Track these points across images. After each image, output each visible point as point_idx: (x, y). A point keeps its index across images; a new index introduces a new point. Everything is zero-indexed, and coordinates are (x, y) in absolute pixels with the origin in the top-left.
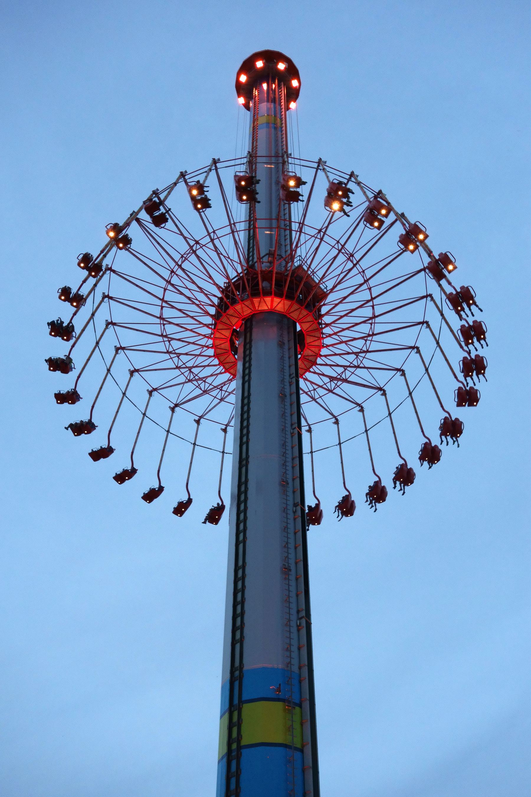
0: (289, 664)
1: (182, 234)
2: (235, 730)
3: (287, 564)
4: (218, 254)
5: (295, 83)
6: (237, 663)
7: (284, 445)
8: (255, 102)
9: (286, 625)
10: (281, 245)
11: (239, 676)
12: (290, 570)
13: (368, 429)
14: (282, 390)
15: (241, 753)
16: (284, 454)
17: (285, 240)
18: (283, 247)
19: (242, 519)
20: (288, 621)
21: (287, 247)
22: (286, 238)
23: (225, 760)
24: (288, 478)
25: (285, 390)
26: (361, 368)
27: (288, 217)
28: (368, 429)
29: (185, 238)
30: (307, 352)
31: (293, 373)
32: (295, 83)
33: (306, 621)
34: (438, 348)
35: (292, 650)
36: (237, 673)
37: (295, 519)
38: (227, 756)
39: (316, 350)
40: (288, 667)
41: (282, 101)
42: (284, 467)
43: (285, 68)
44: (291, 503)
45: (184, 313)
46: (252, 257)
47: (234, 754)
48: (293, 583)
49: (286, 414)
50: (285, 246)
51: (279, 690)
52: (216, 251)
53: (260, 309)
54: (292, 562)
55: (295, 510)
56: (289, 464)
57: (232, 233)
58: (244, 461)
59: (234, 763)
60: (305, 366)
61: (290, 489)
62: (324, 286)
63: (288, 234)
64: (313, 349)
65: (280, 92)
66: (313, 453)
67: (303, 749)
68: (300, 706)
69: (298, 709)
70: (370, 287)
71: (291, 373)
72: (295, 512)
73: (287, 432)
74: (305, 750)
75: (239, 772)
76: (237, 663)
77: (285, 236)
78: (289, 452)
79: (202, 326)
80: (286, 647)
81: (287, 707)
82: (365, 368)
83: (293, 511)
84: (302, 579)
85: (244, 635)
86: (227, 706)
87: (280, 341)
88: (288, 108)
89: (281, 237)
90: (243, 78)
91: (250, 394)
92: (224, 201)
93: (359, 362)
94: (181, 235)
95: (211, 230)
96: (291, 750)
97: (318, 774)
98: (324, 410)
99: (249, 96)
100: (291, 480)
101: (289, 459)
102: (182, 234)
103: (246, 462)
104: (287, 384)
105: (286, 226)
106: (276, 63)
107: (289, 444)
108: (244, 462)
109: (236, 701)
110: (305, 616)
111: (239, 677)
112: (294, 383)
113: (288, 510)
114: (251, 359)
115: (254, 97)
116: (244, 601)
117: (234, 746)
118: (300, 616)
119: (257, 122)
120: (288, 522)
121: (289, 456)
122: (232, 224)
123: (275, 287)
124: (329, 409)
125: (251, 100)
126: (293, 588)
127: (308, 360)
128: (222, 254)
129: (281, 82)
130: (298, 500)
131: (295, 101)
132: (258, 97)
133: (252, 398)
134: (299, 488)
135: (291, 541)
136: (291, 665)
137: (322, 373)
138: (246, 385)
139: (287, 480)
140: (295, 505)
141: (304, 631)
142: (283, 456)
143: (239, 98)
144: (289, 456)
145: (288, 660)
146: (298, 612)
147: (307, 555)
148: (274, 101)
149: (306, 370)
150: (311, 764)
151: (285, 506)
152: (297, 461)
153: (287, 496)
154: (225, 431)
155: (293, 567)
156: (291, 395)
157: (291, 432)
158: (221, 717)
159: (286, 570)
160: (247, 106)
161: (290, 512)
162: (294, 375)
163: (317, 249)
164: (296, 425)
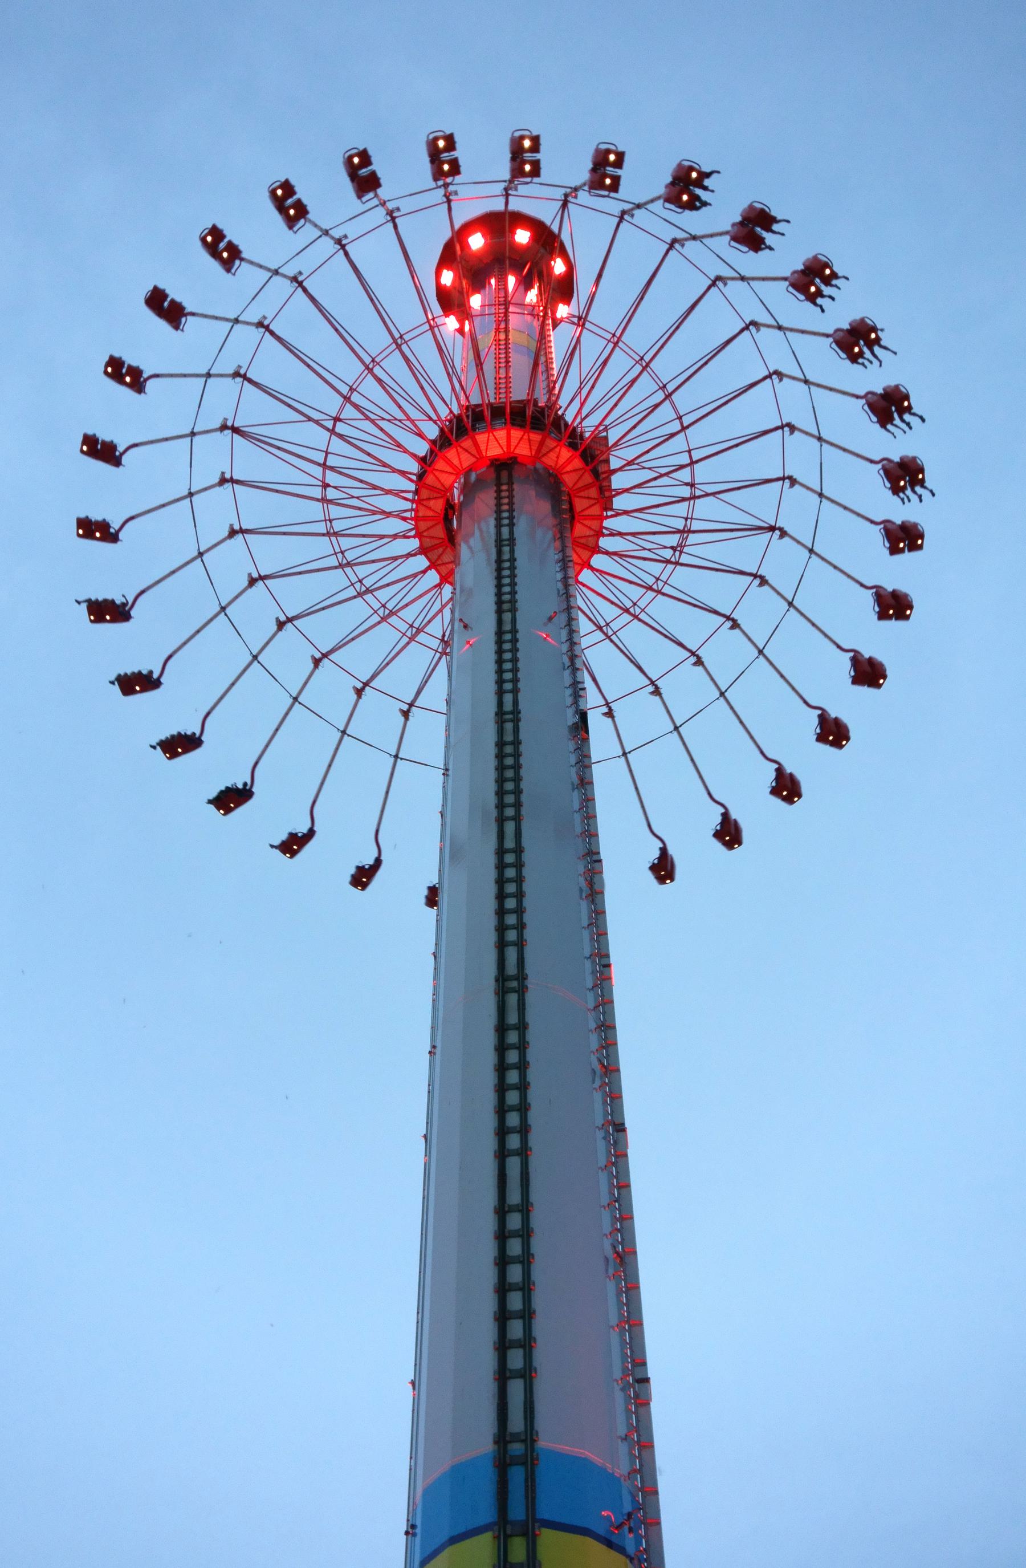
1: (310, 419)
13: (819, 491)
26: (699, 497)
28: (819, 491)
29: (317, 422)
30: (580, 530)
39: (594, 524)
45: (363, 414)
57: (397, 348)
70: (663, 383)
92: (372, 300)
95: (397, 335)
98: (735, 450)
102: (310, 419)
122: (398, 339)
123: (543, 268)
124: (746, 436)
127: (585, 547)
128: (389, 421)
137: (624, 537)
149: (583, 565)
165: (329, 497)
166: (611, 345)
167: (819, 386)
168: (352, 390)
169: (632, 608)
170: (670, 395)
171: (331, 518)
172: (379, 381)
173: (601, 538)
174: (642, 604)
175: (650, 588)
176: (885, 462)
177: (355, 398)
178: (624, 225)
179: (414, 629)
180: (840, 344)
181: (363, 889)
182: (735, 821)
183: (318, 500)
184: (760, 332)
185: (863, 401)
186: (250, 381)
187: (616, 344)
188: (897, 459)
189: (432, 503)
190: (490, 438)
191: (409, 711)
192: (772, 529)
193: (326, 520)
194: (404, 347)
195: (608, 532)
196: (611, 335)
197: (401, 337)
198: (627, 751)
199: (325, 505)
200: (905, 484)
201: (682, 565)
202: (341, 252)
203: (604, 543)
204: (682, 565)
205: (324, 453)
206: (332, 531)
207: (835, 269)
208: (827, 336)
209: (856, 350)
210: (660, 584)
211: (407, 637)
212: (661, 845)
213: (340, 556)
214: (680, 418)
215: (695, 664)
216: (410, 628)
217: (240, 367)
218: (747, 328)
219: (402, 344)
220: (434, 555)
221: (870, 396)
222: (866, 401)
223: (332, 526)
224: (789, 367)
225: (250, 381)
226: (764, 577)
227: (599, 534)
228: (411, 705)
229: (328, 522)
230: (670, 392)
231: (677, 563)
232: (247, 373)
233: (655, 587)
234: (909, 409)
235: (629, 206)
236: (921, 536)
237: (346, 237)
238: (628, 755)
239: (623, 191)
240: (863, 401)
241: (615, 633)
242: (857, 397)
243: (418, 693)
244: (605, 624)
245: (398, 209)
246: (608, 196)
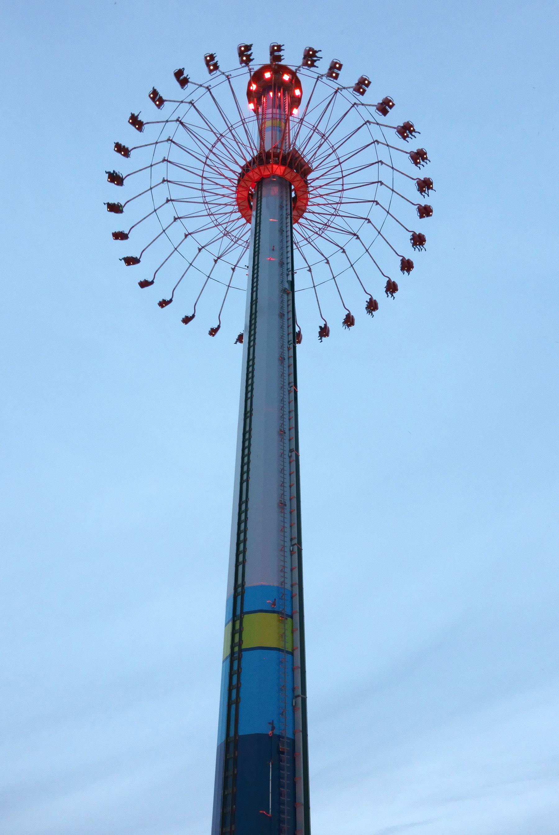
0: (283, 583)
2: (237, 636)
3: (282, 429)
4: (237, 142)
5: (297, 92)
6: (240, 581)
7: (282, 400)
8: (263, 108)
9: (281, 550)
10: (283, 231)
11: (238, 670)
12: (285, 505)
14: (281, 354)
15: (242, 654)
16: (282, 408)
17: (287, 227)
18: (285, 233)
19: (244, 500)
20: (283, 548)
21: (288, 232)
22: (287, 225)
23: (228, 660)
24: (286, 522)
25: (284, 354)
26: (338, 216)
27: (290, 267)
31: (291, 340)
32: (297, 92)
33: (296, 454)
34: (381, 127)
35: (285, 531)
36: (240, 589)
37: (290, 463)
38: (230, 658)
40: (282, 585)
41: (286, 107)
42: (282, 419)
43: (289, 79)
44: (287, 449)
46: (259, 237)
47: (236, 655)
48: (287, 515)
49: (285, 400)
50: (287, 232)
51: (274, 604)
52: (235, 140)
53: (265, 174)
54: (287, 498)
55: (291, 455)
56: (287, 417)
58: (248, 413)
59: (236, 663)
61: (287, 437)
63: (294, 484)
64: (302, 190)
65: (285, 100)
66: (353, 266)
67: (295, 738)
68: (292, 617)
69: (289, 619)
71: (289, 340)
72: (290, 457)
73: (285, 378)
74: (294, 616)
75: (240, 671)
76: (240, 581)
77: (287, 223)
78: (286, 406)
79: (224, 178)
80: (281, 569)
81: (280, 618)
82: (340, 216)
83: (290, 550)
84: (295, 513)
85: (246, 558)
86: (231, 616)
87: (281, 313)
88: (291, 114)
89: (284, 276)
90: (254, 87)
91: (254, 363)
93: (336, 212)
95: (230, 126)
96: (282, 653)
97: (307, 736)
99: (258, 103)
100: (285, 205)
101: (286, 412)
103: (250, 414)
104: (286, 349)
105: (287, 215)
106: (282, 75)
107: (286, 400)
108: (249, 414)
109: (238, 612)
110: (297, 543)
111: (242, 592)
112: (292, 348)
113: (285, 455)
114: (256, 328)
115: (262, 103)
116: (245, 562)
117: (236, 649)
118: (293, 543)
119: (264, 125)
120: (285, 477)
121: (287, 410)
125: (260, 106)
126: (287, 520)
129: (285, 91)
130: (293, 446)
131: (297, 108)
132: (266, 103)
133: (256, 360)
134: (299, 646)
135: (287, 481)
136: (285, 583)
138: (252, 349)
139: (285, 429)
140: (291, 451)
141: (296, 556)
142: (281, 409)
143: (250, 104)
144: (287, 410)
145: (283, 579)
146: (291, 540)
147: (307, 747)
148: (280, 107)
150: (299, 665)
151: (282, 451)
152: (293, 414)
153: (284, 443)
155: (288, 503)
156: (289, 358)
157: (288, 390)
158: (226, 625)
159: (282, 505)
160: (256, 111)
161: (286, 457)
162: (292, 342)
163: (330, 155)
164: (293, 384)
165: (204, 189)
166: (312, 131)
167: (392, 147)
168: (213, 147)
170: (335, 150)
171: (205, 196)
172: (223, 144)
176: (418, 180)
178: (319, 82)
180: (399, 132)
181: (213, 336)
182: (352, 316)
183: (200, 190)
184: (371, 125)
185: (409, 155)
186: (174, 142)
187: (314, 131)
188: (422, 179)
189: (243, 193)
191: (235, 268)
192: (355, 235)
193: (203, 197)
194: (233, 131)
196: (313, 126)
197: (232, 126)
198: (315, 286)
199: (203, 192)
200: (420, 161)
201: (322, 236)
202: (208, 92)
204: (322, 236)
206: (205, 202)
207: (414, 128)
208: (395, 128)
209: (405, 134)
212: (325, 323)
213: (208, 210)
217: (170, 137)
218: (365, 123)
219: (232, 130)
220: (243, 212)
221: (412, 153)
222: (410, 155)
224: (381, 140)
225: (174, 142)
226: (369, 219)
228: (235, 266)
229: (204, 198)
230: (335, 149)
231: (320, 235)
232: (173, 139)
234: (414, 130)
235: (341, 87)
236: (432, 211)
237: (210, 86)
238: (316, 287)
239: (339, 80)
240: (409, 155)
242: (407, 153)
243: (238, 262)
244: (308, 237)
245: (230, 75)
246: (333, 81)
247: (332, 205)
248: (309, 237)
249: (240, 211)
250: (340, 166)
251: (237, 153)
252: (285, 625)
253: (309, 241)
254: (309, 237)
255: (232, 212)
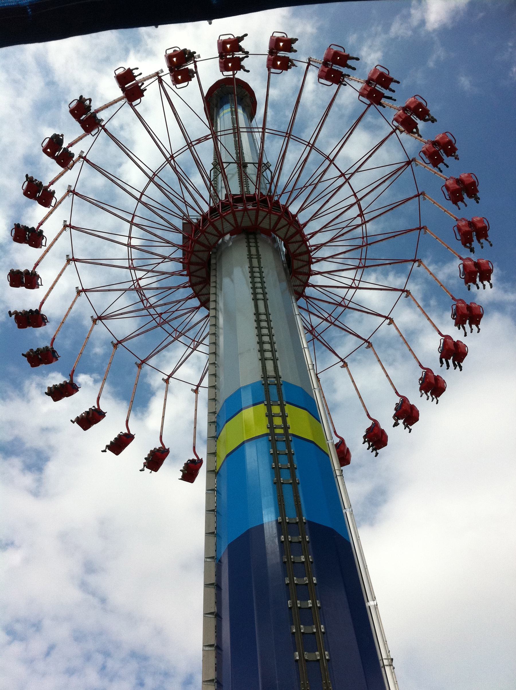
60: (301, 280)
62: (194, 149)
92: (149, 132)
94: (126, 291)
154: (196, 391)
163: (340, 187)
169: (329, 317)
173: (312, 265)
174: (348, 297)
175: (351, 287)
177: (156, 179)
179: (195, 342)
190: (245, 215)
195: (315, 260)
199: (129, 248)
203: (315, 267)
205: (132, 215)
210: (357, 282)
211: (191, 348)
214: (355, 195)
215: (342, 367)
216: (193, 342)
220: (198, 288)
223: (132, 263)
227: (310, 262)
229: (130, 260)
233: (353, 285)
241: (319, 335)
247: (296, 188)
248: (330, 315)
249: (192, 285)
250: (347, 183)
251: (178, 216)
252: (174, 245)
253: (330, 321)
254: (330, 315)
255: (178, 287)
